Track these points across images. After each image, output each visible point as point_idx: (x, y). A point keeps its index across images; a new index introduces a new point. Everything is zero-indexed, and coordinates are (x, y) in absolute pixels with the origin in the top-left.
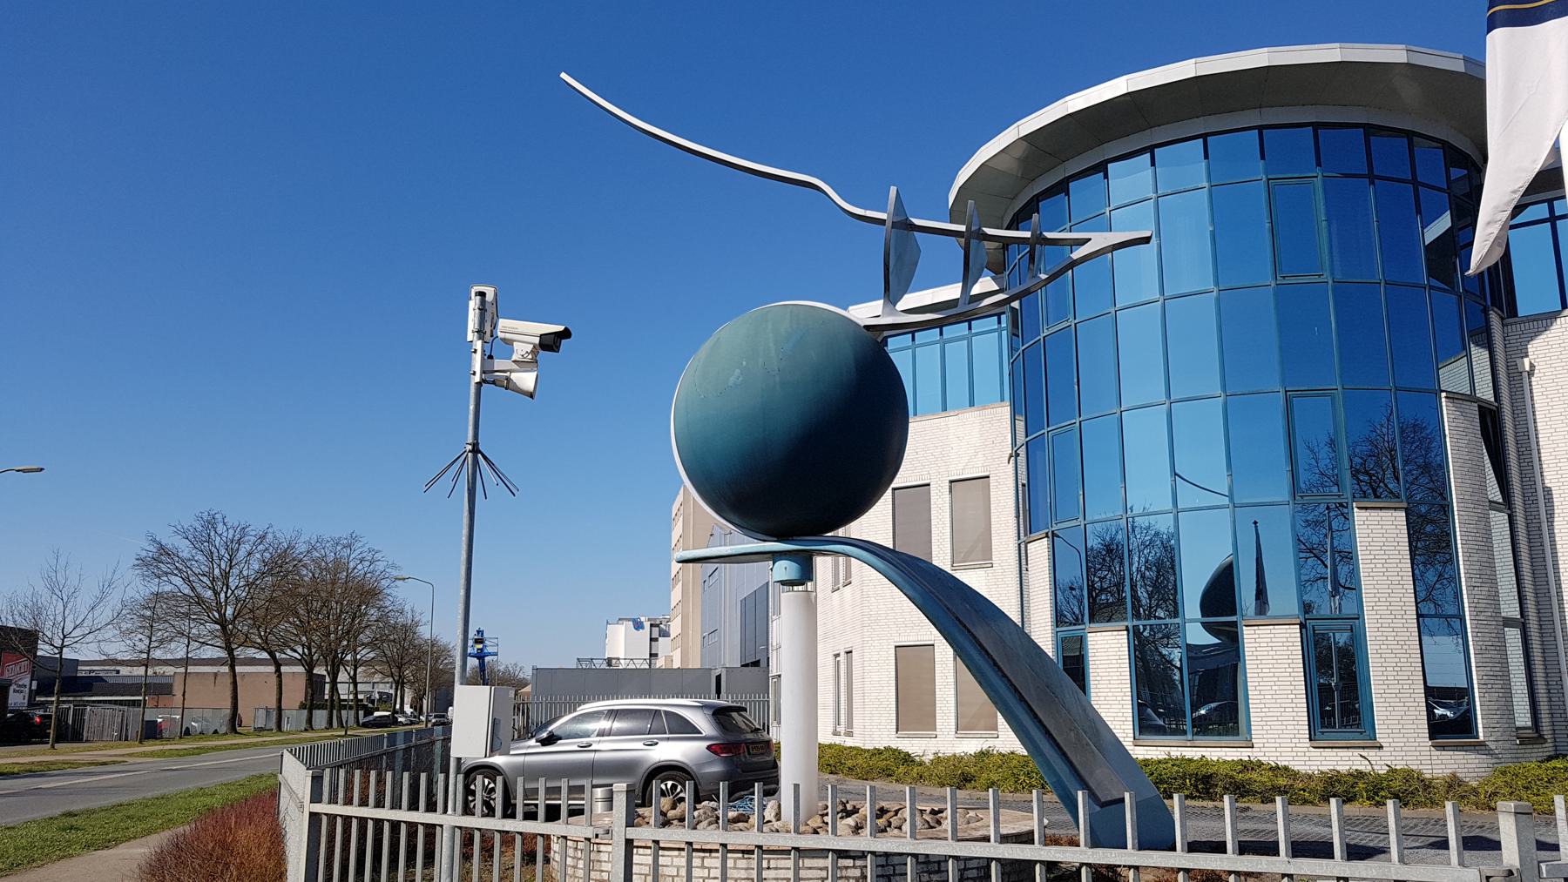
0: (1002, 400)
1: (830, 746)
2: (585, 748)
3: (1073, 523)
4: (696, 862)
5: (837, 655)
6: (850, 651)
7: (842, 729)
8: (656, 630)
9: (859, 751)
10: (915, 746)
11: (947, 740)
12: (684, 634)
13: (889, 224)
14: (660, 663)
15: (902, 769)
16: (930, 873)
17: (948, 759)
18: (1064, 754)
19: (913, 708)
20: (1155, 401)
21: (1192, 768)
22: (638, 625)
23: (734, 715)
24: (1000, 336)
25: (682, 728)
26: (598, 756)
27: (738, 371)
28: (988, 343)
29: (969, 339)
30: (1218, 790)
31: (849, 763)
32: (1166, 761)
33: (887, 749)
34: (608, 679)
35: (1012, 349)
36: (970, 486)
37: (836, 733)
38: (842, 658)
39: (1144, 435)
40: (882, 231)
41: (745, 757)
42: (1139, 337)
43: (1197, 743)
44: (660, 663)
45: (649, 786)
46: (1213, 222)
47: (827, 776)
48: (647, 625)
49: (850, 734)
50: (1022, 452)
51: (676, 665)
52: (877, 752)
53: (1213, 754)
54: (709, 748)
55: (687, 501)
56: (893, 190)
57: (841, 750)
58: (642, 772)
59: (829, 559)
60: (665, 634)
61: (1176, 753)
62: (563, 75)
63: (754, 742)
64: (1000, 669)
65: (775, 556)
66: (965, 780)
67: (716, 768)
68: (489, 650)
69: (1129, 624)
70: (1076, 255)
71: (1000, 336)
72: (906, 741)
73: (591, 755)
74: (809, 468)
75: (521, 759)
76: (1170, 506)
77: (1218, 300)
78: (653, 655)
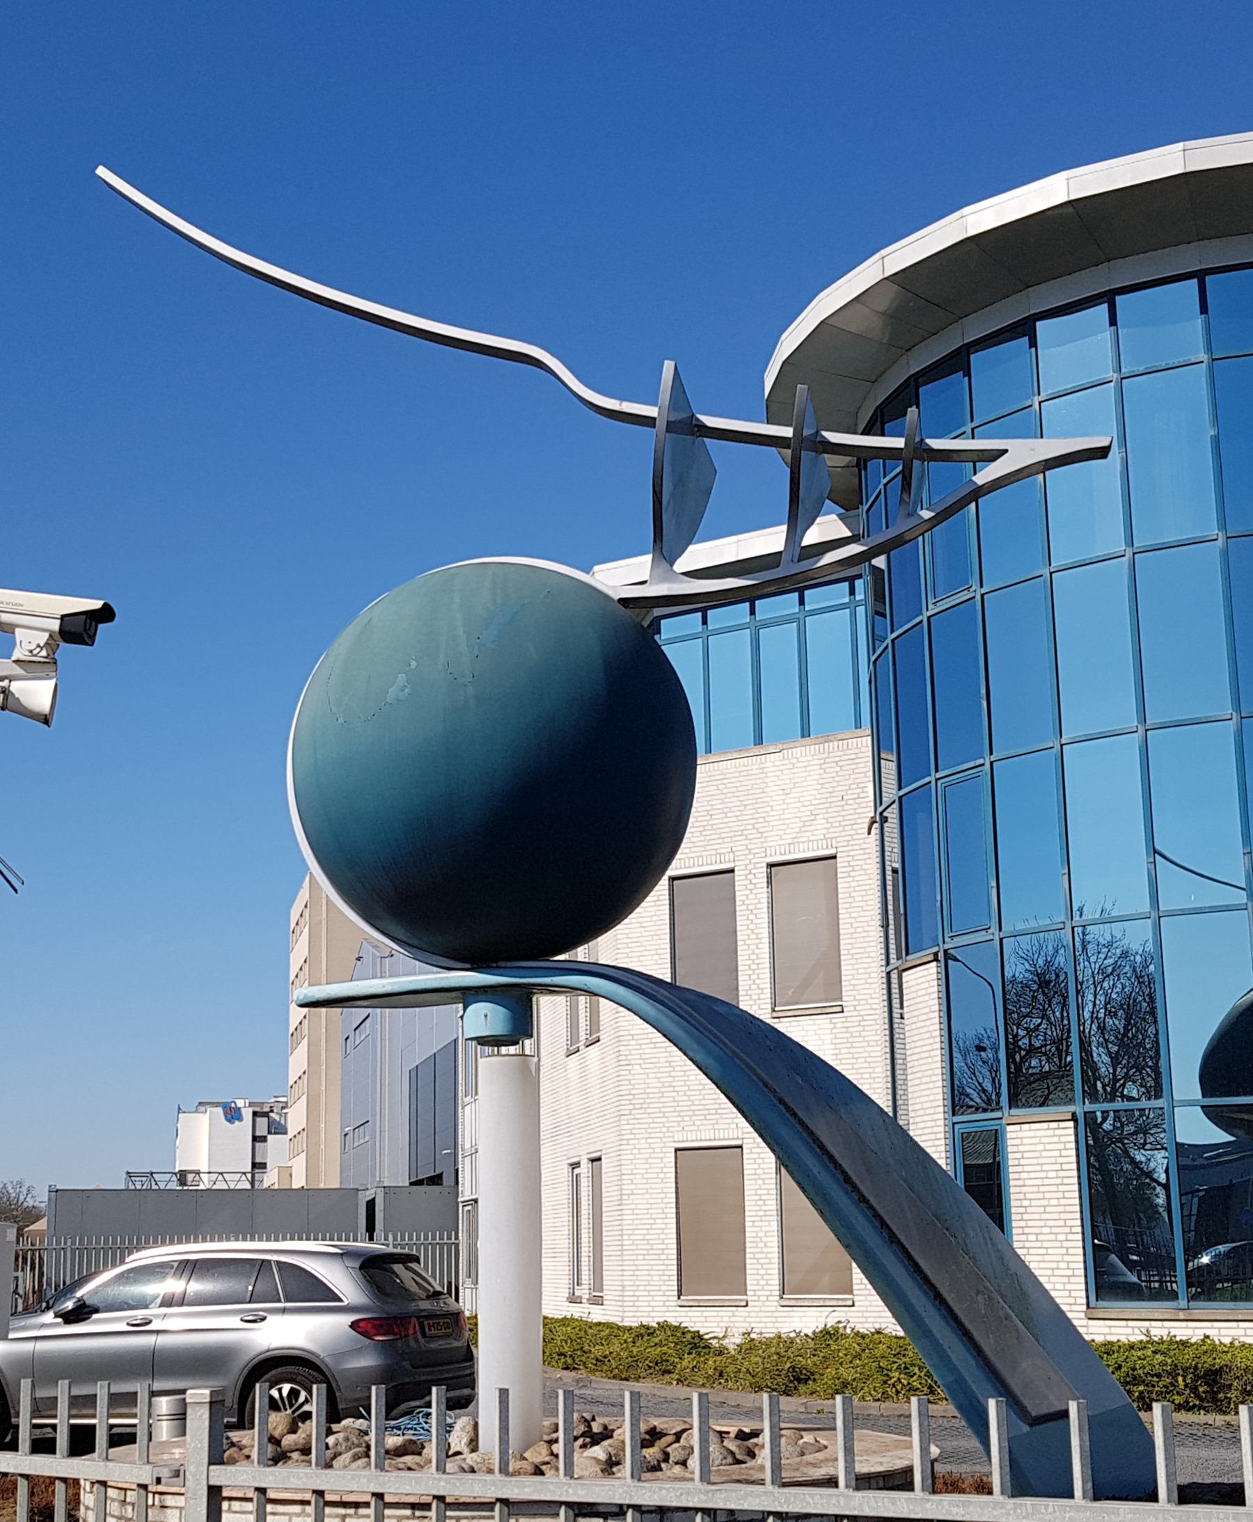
0: (858, 725)
1: (564, 1322)
2: (141, 1327)
5: (576, 1165)
7: (584, 1292)
8: (262, 1123)
9: (612, 1330)
10: (714, 1321)
11: (762, 1311)
12: (310, 1130)
13: (661, 425)
14: (270, 1179)
17: (767, 1343)
19: (707, 1254)
21: (1187, 1358)
22: (232, 1114)
23: (398, 1268)
24: (854, 615)
25: (307, 1291)
26: (162, 1340)
27: (402, 678)
31: (597, 1351)
32: (1142, 1346)
33: (663, 1326)
34: (179, 1207)
37: (574, 1299)
39: (1102, 784)
41: (416, 1342)
42: (1090, 616)
43: (1197, 1314)
44: (270, 1179)
45: (249, 1392)
46: (1216, 420)
47: (559, 1374)
48: (247, 1114)
49: (597, 1301)
50: (892, 814)
51: (298, 1182)
52: (646, 1332)
54: (354, 1325)
56: (669, 366)
57: (583, 1328)
60: (278, 1129)
61: (1159, 1331)
62: (102, 171)
63: (432, 1316)
64: (855, 1188)
65: (467, 995)
67: (367, 1361)
69: (1079, 1109)
70: (985, 475)
71: (854, 615)
72: (695, 1312)
75: (28, 1347)
76: (1146, 907)
77: (1225, 553)
78: (258, 1166)
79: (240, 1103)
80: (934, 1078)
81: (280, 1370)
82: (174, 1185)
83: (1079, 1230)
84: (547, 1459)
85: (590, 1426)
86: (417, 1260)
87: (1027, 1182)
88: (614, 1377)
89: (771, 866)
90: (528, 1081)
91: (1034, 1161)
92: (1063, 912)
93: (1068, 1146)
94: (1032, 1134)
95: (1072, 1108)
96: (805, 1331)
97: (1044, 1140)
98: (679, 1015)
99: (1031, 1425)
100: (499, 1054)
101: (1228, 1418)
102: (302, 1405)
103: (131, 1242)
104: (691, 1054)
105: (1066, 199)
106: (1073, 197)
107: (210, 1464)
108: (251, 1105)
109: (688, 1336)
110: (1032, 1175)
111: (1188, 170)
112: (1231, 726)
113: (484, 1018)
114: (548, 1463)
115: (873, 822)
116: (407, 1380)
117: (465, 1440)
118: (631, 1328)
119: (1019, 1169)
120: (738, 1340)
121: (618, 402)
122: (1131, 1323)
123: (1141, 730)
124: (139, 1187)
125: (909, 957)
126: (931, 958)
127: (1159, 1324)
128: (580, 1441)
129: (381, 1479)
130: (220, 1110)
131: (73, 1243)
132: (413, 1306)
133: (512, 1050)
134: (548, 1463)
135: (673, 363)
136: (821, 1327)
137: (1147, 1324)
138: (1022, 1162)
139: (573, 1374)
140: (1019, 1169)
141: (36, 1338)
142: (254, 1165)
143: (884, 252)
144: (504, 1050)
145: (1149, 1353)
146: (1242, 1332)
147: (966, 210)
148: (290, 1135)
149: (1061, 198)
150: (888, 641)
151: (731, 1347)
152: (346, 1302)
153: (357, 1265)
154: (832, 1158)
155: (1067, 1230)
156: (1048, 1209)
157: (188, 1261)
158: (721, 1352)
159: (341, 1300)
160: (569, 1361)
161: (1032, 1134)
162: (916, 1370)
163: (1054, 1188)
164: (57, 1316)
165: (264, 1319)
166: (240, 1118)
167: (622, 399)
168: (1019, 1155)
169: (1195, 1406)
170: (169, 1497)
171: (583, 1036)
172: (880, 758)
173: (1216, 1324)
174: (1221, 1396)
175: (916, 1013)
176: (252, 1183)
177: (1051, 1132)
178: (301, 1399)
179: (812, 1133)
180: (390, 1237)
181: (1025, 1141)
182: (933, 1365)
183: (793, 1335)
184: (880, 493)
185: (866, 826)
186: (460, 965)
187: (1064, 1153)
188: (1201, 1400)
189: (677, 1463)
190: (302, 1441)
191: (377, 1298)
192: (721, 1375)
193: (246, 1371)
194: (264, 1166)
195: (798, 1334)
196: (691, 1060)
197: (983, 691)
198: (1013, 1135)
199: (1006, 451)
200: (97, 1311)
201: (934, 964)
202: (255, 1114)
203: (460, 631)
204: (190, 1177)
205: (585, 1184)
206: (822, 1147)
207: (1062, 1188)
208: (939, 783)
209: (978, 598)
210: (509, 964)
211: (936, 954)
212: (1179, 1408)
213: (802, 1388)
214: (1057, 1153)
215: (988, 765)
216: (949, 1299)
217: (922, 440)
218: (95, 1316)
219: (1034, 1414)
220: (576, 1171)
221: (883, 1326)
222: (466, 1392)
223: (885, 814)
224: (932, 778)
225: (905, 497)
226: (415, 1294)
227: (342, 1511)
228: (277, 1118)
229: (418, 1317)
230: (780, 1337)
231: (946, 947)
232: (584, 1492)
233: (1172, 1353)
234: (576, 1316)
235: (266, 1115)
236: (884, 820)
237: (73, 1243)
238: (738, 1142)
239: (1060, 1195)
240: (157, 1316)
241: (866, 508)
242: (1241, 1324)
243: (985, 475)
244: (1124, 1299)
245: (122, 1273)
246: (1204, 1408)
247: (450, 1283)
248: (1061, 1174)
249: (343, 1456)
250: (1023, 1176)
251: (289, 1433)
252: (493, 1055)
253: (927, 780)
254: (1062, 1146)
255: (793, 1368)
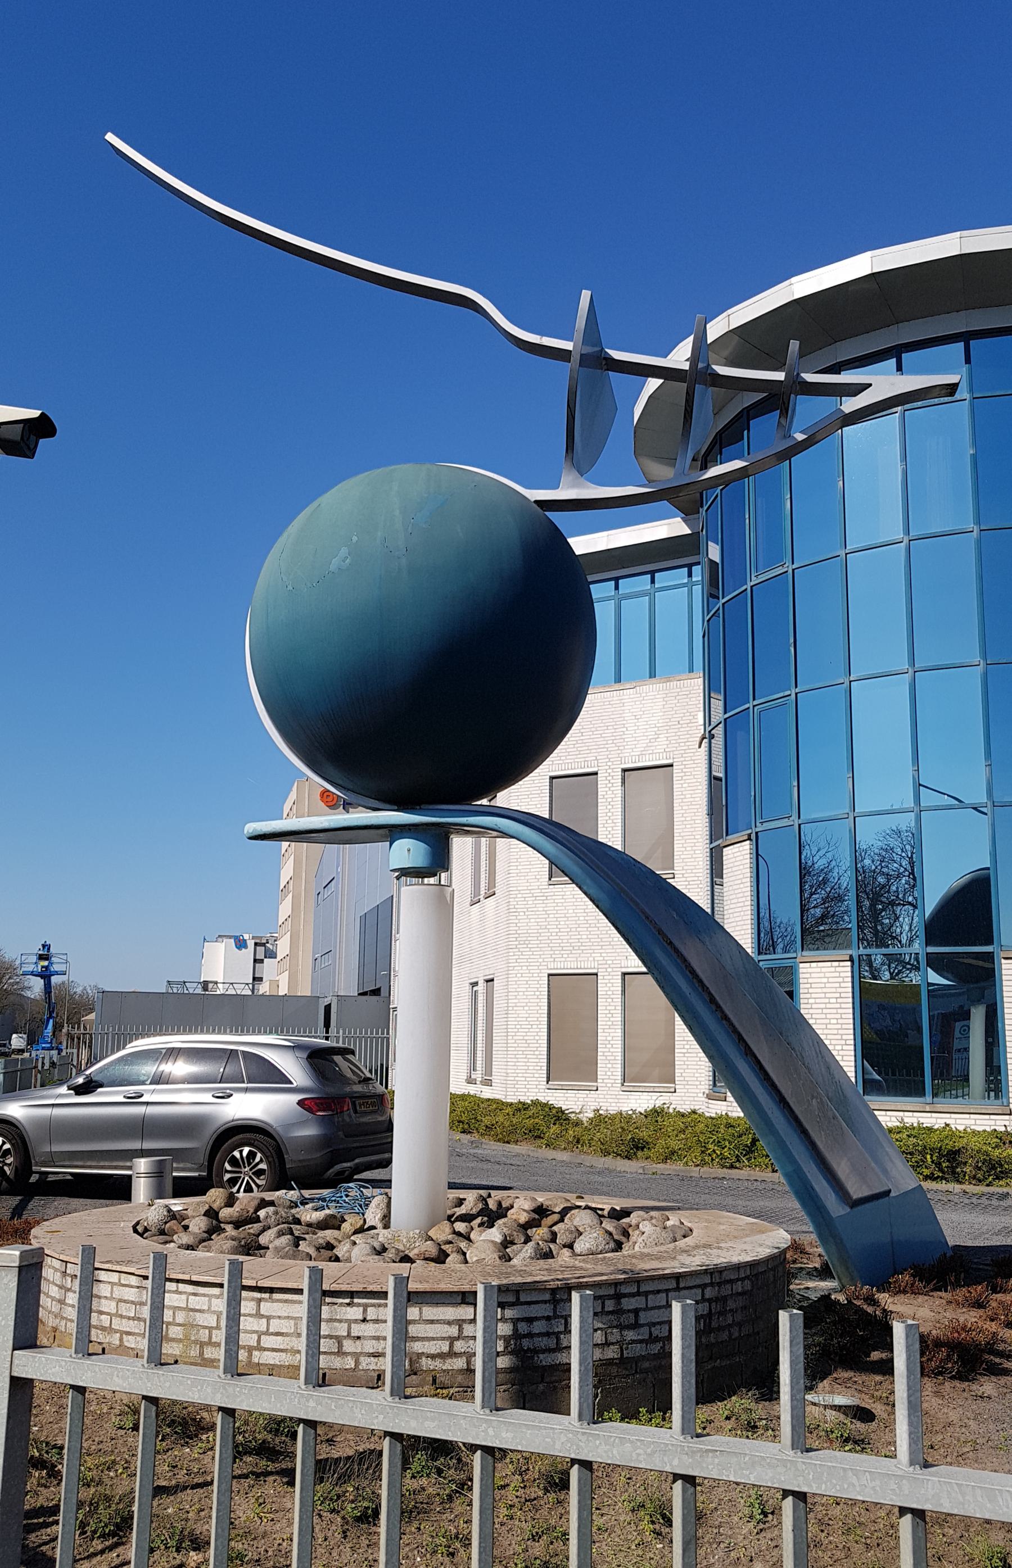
0: (691, 670)
1: (464, 1097)
2: (134, 1100)
3: (785, 822)
4: (247, 1306)
5: (476, 984)
6: (501, 968)
7: (478, 1075)
8: (261, 950)
9: (498, 1105)
10: (575, 1101)
11: (608, 1095)
12: (292, 956)
13: (576, 358)
14: (264, 988)
15: (554, 1129)
16: (622, 1327)
17: (612, 1118)
18: (804, 1132)
19: (569, 1051)
20: (894, 669)
21: (933, 1140)
22: (241, 944)
23: (338, 1059)
24: (690, 593)
25: (265, 1075)
26: (151, 1110)
27: (344, 551)
28: (677, 599)
29: (651, 595)
30: (968, 1169)
31: (487, 1121)
32: (899, 1131)
33: (536, 1103)
34: (192, 1006)
35: (707, 608)
36: (647, 777)
37: (470, 1081)
38: (481, 988)
39: (880, 711)
40: (564, 370)
41: (348, 1116)
42: (876, 589)
43: (939, 1107)
44: (264, 988)
45: (210, 1160)
46: (975, 443)
47: (459, 1136)
48: (251, 944)
49: (488, 1083)
50: (719, 732)
51: (283, 991)
52: (522, 1107)
53: (960, 1122)
54: (300, 1103)
55: (304, 797)
56: (586, 295)
57: (476, 1102)
58: (208, 1135)
59: (469, 840)
60: (271, 955)
61: (911, 1119)
62: (110, 137)
63: (363, 1096)
64: (718, 1007)
65: (393, 832)
66: (635, 1148)
67: (310, 1131)
68: (56, 968)
69: (855, 954)
70: (850, 405)
71: (690, 593)
72: (559, 1094)
73: (140, 1110)
74: (442, 712)
75: (47, 1111)
76: (911, 804)
77: (979, 542)
78: (257, 979)
79: (246, 937)
80: (745, 927)
81: (241, 1136)
82: (199, 991)
83: (852, 1042)
84: (450, 1237)
85: (487, 1204)
86: (353, 1053)
87: (814, 1006)
88: (499, 1140)
89: (624, 770)
90: (443, 908)
91: (820, 990)
92: (848, 806)
93: (846, 980)
94: (819, 970)
95: (850, 952)
96: (639, 1110)
97: (827, 975)
98: (577, 855)
99: (851, 1208)
100: (423, 884)
101: (963, 1187)
102: (258, 1164)
103: (137, 1029)
104: (585, 888)
105: (868, 272)
106: (875, 270)
107: (14, 1349)
108: (253, 938)
109: (554, 1111)
110: (818, 1001)
111: (963, 252)
112: (980, 669)
113: (407, 852)
114: (450, 1242)
115: (703, 738)
116: (341, 1146)
117: (379, 1216)
118: (512, 1104)
119: (808, 996)
120: (591, 1115)
121: (539, 337)
122: (889, 1113)
123: (911, 671)
124: (175, 991)
125: (729, 837)
126: (746, 837)
127: (910, 1114)
128: (479, 1220)
129: (230, 1390)
130: (232, 940)
131: (114, 1030)
132: (348, 1089)
133: (432, 880)
134: (450, 1242)
135: (589, 293)
136: (651, 1107)
137: (901, 1114)
138: (811, 991)
139: (469, 1136)
140: (808, 996)
141: (53, 1105)
142: (254, 979)
143: (729, 311)
144: (426, 880)
145: (905, 1136)
146: (973, 1122)
147: (794, 280)
148: (279, 958)
149: (866, 271)
150: (720, 604)
151: (584, 1119)
152: (295, 1084)
153: (305, 1056)
154: (701, 981)
155: (843, 1042)
156: (829, 1026)
157: (173, 1048)
158: (578, 1123)
159: (291, 1083)
160: (466, 1126)
161: (819, 970)
162: (727, 1143)
163: (835, 1011)
164: (69, 1089)
165: (231, 1095)
166: (246, 947)
167: (542, 334)
168: (809, 986)
169: (938, 1177)
170: (103, 1272)
171: (482, 892)
172: (710, 697)
173: (953, 1116)
174: (959, 1170)
175: (733, 878)
176: (253, 991)
177: (833, 969)
178: (258, 1159)
179: (685, 960)
180: (341, 1031)
181: (813, 975)
182: (776, 1158)
183: (630, 1112)
184: (717, 496)
185: (698, 739)
186: (388, 806)
187: (843, 985)
188: (943, 1172)
189: (565, 1246)
190: (236, 1214)
191: (320, 1082)
192: (578, 1142)
193: (215, 1136)
194: (261, 979)
195: (634, 1111)
196: (585, 893)
197: (792, 640)
198: (804, 971)
199: (870, 385)
200: (101, 1086)
201: (748, 842)
202: (256, 944)
203: (397, 513)
204: (210, 985)
205: (481, 998)
206: (693, 972)
207: (840, 1011)
208: (756, 708)
209: (790, 571)
210: (431, 807)
211: (749, 835)
212: (926, 1178)
213: (640, 1153)
214: (837, 985)
215: (793, 696)
216: (792, 1104)
217: (798, 374)
218: (100, 1090)
219: (854, 1198)
220: (475, 988)
221: (697, 1107)
222: (387, 1155)
223: (713, 732)
224: (750, 705)
225: (783, 421)
226: (349, 1079)
227: (257, 1295)
228: (271, 947)
229: (351, 1098)
230: (621, 1114)
231: (757, 830)
232: (510, 1435)
233: (921, 1137)
234: (472, 1093)
235: (264, 945)
236: (712, 737)
237: (114, 1030)
238: (595, 971)
239: (838, 1016)
240: (147, 1091)
241: (705, 508)
242: (972, 1116)
243: (850, 405)
244: (878, 1095)
245: (122, 1057)
246: (945, 1179)
247: (382, 1065)
248: (839, 1000)
249: (270, 1232)
250: (811, 1001)
251: (226, 1206)
252: (418, 884)
253: (746, 706)
254: (841, 980)
255: (633, 1138)
